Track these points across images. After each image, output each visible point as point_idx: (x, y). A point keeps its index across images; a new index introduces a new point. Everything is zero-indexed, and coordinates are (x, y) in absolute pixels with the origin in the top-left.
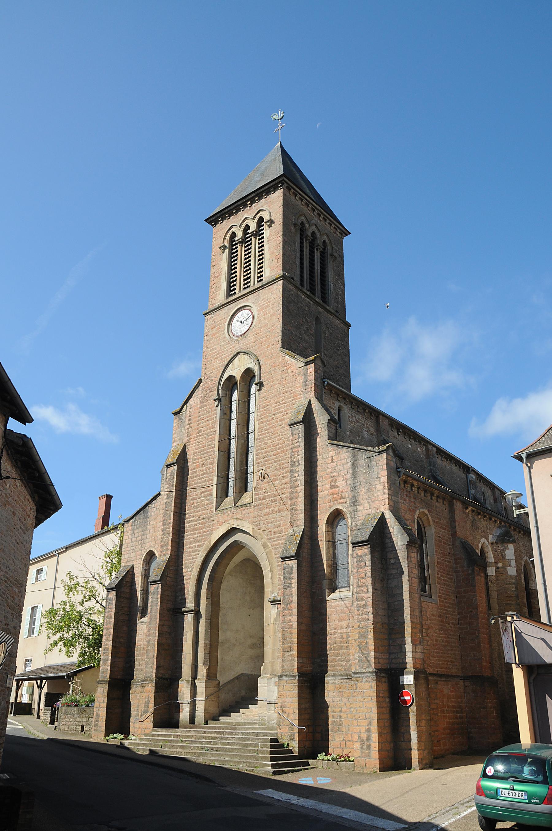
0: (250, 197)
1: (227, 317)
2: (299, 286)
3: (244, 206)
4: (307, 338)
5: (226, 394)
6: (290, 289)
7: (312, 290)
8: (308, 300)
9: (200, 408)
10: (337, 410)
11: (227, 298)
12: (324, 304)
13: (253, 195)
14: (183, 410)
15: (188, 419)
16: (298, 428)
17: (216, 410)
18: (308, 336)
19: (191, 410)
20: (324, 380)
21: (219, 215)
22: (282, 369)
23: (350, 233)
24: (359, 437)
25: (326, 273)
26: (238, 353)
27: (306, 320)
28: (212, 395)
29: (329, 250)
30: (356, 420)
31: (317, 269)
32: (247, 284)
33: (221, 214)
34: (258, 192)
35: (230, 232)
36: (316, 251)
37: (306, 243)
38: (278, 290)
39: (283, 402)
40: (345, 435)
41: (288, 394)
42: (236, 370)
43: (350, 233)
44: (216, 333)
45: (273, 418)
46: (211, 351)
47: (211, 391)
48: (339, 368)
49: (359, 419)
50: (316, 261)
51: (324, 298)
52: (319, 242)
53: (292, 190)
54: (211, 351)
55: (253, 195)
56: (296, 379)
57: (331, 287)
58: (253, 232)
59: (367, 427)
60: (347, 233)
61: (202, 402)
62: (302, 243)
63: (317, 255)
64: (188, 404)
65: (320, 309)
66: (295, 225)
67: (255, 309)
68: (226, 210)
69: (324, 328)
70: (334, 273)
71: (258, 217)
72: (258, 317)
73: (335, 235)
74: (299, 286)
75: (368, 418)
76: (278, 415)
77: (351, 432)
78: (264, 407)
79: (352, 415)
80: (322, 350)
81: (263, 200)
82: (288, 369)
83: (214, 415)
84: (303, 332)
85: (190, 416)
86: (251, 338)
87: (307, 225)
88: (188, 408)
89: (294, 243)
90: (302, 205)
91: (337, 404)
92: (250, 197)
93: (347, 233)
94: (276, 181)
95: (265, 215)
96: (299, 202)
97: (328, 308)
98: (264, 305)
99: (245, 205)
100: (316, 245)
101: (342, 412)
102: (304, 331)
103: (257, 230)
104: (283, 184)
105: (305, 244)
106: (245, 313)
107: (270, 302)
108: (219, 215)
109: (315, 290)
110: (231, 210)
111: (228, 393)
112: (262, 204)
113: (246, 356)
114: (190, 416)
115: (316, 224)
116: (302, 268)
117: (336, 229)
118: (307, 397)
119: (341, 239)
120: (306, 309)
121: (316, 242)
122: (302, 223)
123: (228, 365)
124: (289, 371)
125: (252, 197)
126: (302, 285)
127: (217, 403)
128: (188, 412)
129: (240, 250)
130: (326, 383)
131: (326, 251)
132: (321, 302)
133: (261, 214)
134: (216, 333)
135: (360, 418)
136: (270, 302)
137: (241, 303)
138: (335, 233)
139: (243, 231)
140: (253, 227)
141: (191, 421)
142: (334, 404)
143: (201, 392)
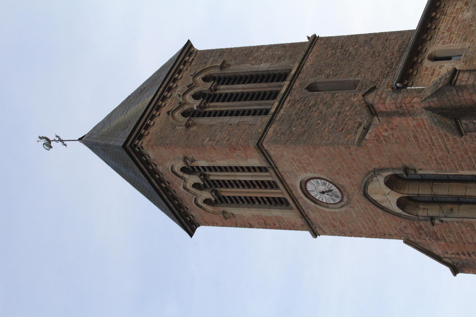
0: (156, 185)
1: (318, 209)
2: (266, 119)
3: (168, 191)
4: (337, 104)
5: (424, 209)
6: (274, 132)
7: (273, 95)
8: (286, 103)
9: (445, 241)
10: (436, 63)
11: (291, 209)
12: (289, 78)
13: (153, 181)
14: (450, 262)
15: (462, 256)
16: (465, 124)
17: (447, 222)
18: (334, 103)
19: (450, 252)
20: (395, 88)
21: (183, 220)
22: (384, 142)
23: (189, 41)
24: (471, 25)
25: (247, 74)
26: (366, 195)
27: (313, 106)
28: (427, 227)
29: (215, 72)
30: (448, 31)
31: (243, 88)
32: (272, 185)
33: (181, 218)
34: (149, 175)
35: (204, 205)
36: (218, 92)
37: (209, 107)
38: (277, 149)
39: (429, 141)
40: (470, 50)
41: (418, 135)
42: (390, 199)
43: (189, 41)
44: (341, 222)
45: (454, 153)
46: (365, 228)
47: (421, 228)
48: (374, 52)
49: (446, 26)
50: (231, 91)
51: (281, 76)
52: (206, 87)
53: (143, 131)
54: (365, 228)
55: (153, 181)
56: (396, 126)
57: (264, 67)
58: (201, 179)
59: (456, 13)
60: (189, 45)
61: (438, 239)
62: (210, 114)
63: (224, 89)
64: (442, 256)
65: (297, 84)
66: (188, 126)
67: (304, 176)
68: (176, 212)
69: (321, 79)
70: (245, 63)
71: (181, 174)
72: (315, 172)
73: (193, 63)
74: (266, 119)
75: (443, 11)
76: (449, 147)
77: (465, 40)
78: (438, 163)
79: (441, 39)
80: (351, 79)
81: (160, 168)
82: (384, 136)
83: (454, 225)
84: (330, 110)
85: (458, 254)
86: (344, 181)
87: (186, 107)
88: (446, 255)
89: (211, 126)
90: (160, 114)
91: (427, 63)
92: (156, 185)
93: (189, 45)
94: (133, 154)
95: (179, 165)
96: (157, 120)
97: (293, 72)
98: (297, 166)
99: (167, 190)
100: (210, 92)
101: (438, 55)
102: (328, 108)
103: (199, 174)
104: (135, 146)
105: (211, 109)
106: (310, 187)
107: (293, 159)
108: (183, 220)
109: (271, 92)
110: (174, 206)
111: (421, 207)
112: (163, 168)
113: (370, 187)
114: (458, 254)
115: (183, 95)
116: (243, 113)
117: (186, 62)
118: (420, 111)
119: (198, 53)
120: (298, 106)
121: (206, 92)
122: (184, 114)
123: (383, 208)
124: (385, 134)
125: (157, 182)
126: (267, 112)
127: (437, 222)
128: (453, 256)
129: (226, 192)
130: (398, 85)
131: (217, 76)
132: (287, 83)
133: (177, 170)
134: (341, 222)
135: (444, 24)
136: (293, 159)
137: (299, 193)
138: (191, 63)
139: (201, 190)
140: (195, 179)
141: (465, 253)
142: (427, 69)
143: (423, 241)
